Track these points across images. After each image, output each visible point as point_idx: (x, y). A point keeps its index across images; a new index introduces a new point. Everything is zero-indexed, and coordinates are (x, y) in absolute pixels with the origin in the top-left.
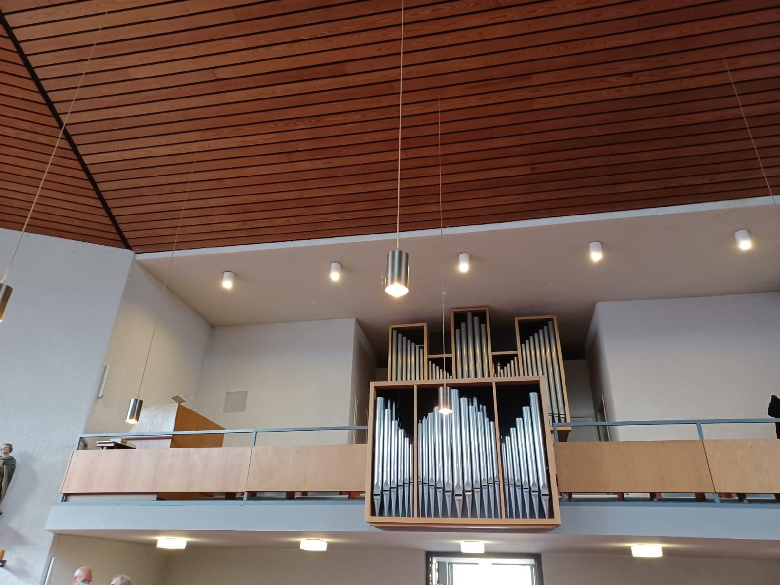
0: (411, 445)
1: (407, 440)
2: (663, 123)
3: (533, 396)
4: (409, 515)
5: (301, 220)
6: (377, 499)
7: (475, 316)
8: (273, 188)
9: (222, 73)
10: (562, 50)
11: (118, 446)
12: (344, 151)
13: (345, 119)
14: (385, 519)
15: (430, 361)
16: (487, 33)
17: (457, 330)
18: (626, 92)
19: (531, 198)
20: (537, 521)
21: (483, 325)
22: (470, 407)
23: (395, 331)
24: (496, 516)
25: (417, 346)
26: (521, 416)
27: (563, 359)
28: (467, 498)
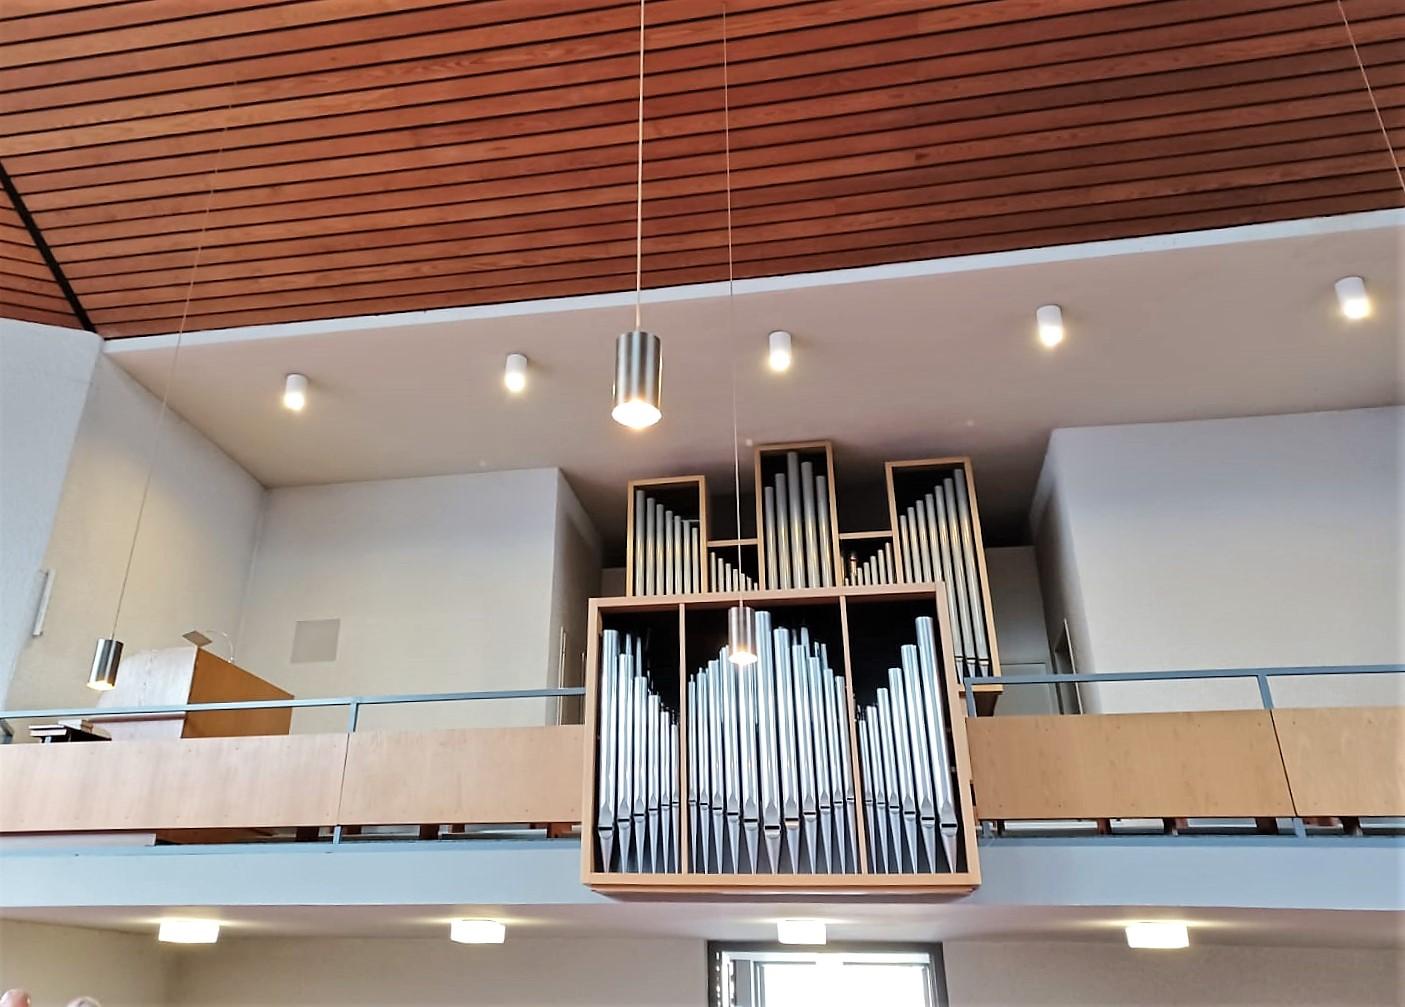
1: (665, 715)
2: (1185, 59)
3: (923, 623)
4: (671, 870)
5: (443, 267)
6: (606, 838)
7: (804, 461)
8: (384, 201)
11: (75, 735)
13: (530, 57)
14: (623, 877)
15: (713, 554)
17: (768, 490)
19: (913, 216)
20: (933, 878)
21: (820, 479)
22: (795, 647)
23: (640, 493)
25: (686, 523)
26: (899, 664)
27: (985, 547)
28: (789, 832)
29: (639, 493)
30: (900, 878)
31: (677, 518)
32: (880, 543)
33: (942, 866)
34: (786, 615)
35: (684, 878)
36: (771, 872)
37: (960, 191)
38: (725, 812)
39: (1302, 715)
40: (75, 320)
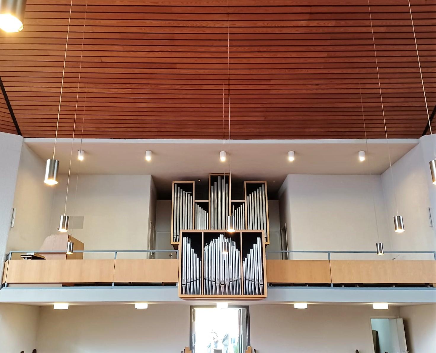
0: (200, 261)
1: (198, 259)
2: (330, 105)
3: (259, 239)
4: (199, 294)
5: (134, 129)
6: (184, 286)
7: (226, 183)
8: (121, 113)
9: (104, 60)
10: (287, 72)
11: (34, 258)
12: (167, 101)
13: (171, 87)
14: (188, 296)
15: (196, 204)
16: (252, 61)
17: (212, 187)
18: (315, 91)
19: (262, 130)
20: (257, 296)
21: (227, 185)
22: (233, 246)
23: (176, 185)
24: (239, 294)
25: (186, 193)
28: (226, 286)
29: (176, 185)
30: (250, 296)
31: (204, 210)
32: (241, 203)
33: (259, 293)
34: (227, 235)
35: (202, 296)
36: (226, 294)
37: (274, 126)
38: (215, 283)
39: (336, 262)
40: (17, 132)
